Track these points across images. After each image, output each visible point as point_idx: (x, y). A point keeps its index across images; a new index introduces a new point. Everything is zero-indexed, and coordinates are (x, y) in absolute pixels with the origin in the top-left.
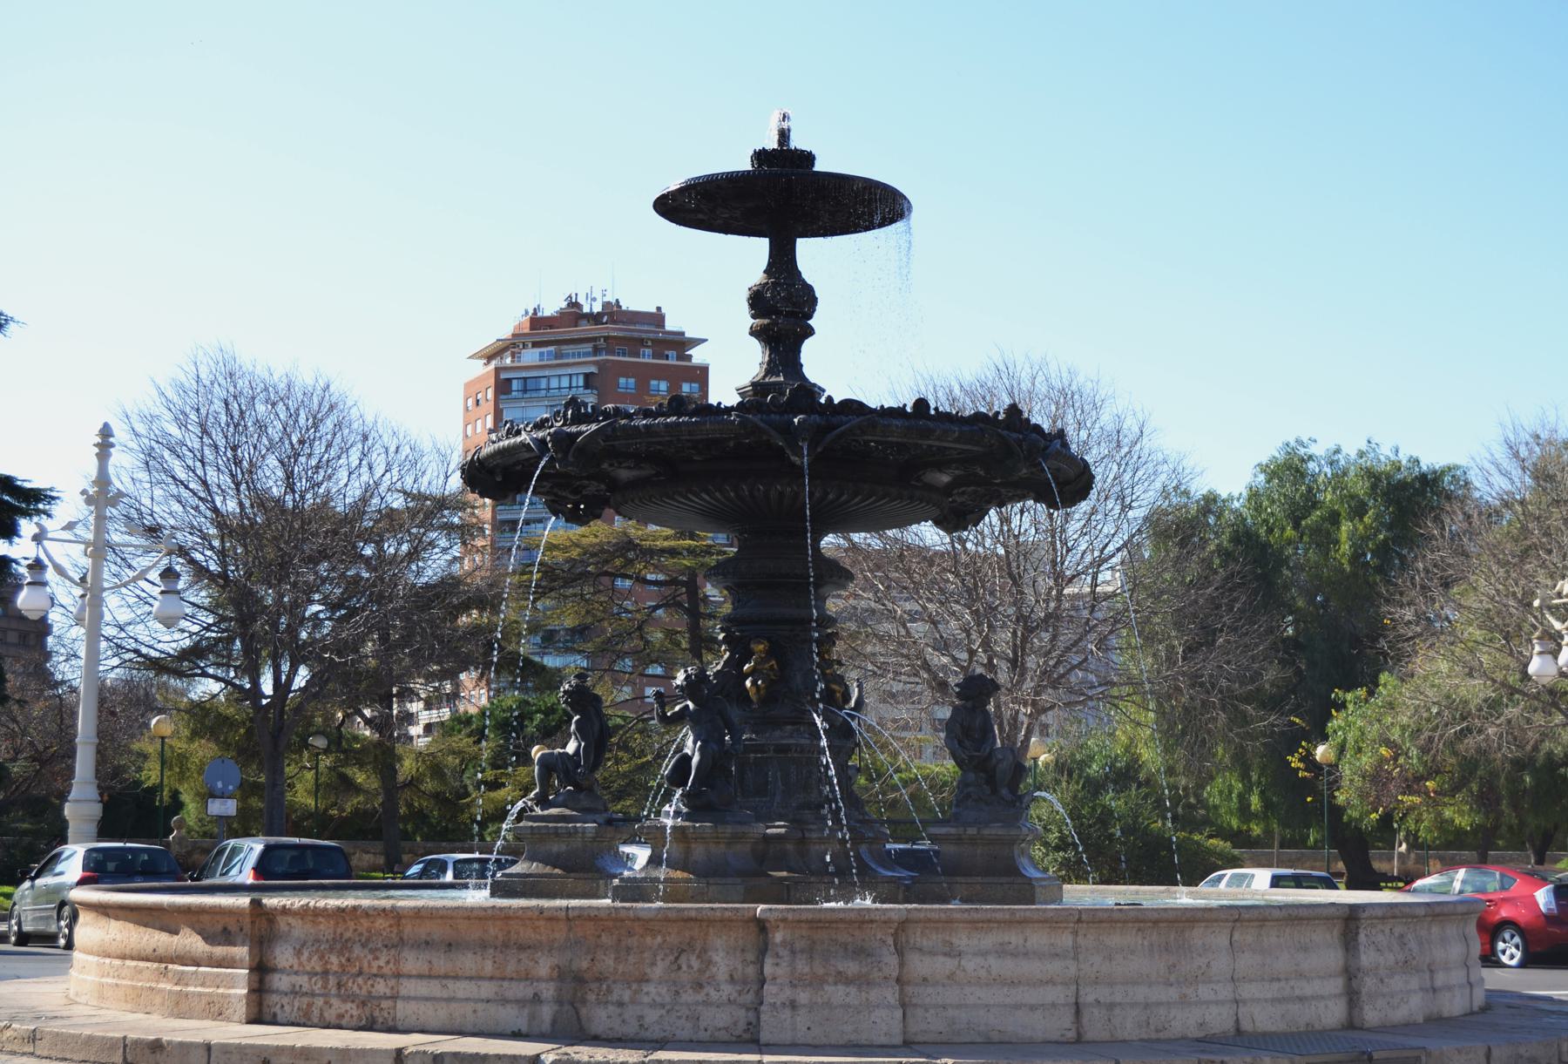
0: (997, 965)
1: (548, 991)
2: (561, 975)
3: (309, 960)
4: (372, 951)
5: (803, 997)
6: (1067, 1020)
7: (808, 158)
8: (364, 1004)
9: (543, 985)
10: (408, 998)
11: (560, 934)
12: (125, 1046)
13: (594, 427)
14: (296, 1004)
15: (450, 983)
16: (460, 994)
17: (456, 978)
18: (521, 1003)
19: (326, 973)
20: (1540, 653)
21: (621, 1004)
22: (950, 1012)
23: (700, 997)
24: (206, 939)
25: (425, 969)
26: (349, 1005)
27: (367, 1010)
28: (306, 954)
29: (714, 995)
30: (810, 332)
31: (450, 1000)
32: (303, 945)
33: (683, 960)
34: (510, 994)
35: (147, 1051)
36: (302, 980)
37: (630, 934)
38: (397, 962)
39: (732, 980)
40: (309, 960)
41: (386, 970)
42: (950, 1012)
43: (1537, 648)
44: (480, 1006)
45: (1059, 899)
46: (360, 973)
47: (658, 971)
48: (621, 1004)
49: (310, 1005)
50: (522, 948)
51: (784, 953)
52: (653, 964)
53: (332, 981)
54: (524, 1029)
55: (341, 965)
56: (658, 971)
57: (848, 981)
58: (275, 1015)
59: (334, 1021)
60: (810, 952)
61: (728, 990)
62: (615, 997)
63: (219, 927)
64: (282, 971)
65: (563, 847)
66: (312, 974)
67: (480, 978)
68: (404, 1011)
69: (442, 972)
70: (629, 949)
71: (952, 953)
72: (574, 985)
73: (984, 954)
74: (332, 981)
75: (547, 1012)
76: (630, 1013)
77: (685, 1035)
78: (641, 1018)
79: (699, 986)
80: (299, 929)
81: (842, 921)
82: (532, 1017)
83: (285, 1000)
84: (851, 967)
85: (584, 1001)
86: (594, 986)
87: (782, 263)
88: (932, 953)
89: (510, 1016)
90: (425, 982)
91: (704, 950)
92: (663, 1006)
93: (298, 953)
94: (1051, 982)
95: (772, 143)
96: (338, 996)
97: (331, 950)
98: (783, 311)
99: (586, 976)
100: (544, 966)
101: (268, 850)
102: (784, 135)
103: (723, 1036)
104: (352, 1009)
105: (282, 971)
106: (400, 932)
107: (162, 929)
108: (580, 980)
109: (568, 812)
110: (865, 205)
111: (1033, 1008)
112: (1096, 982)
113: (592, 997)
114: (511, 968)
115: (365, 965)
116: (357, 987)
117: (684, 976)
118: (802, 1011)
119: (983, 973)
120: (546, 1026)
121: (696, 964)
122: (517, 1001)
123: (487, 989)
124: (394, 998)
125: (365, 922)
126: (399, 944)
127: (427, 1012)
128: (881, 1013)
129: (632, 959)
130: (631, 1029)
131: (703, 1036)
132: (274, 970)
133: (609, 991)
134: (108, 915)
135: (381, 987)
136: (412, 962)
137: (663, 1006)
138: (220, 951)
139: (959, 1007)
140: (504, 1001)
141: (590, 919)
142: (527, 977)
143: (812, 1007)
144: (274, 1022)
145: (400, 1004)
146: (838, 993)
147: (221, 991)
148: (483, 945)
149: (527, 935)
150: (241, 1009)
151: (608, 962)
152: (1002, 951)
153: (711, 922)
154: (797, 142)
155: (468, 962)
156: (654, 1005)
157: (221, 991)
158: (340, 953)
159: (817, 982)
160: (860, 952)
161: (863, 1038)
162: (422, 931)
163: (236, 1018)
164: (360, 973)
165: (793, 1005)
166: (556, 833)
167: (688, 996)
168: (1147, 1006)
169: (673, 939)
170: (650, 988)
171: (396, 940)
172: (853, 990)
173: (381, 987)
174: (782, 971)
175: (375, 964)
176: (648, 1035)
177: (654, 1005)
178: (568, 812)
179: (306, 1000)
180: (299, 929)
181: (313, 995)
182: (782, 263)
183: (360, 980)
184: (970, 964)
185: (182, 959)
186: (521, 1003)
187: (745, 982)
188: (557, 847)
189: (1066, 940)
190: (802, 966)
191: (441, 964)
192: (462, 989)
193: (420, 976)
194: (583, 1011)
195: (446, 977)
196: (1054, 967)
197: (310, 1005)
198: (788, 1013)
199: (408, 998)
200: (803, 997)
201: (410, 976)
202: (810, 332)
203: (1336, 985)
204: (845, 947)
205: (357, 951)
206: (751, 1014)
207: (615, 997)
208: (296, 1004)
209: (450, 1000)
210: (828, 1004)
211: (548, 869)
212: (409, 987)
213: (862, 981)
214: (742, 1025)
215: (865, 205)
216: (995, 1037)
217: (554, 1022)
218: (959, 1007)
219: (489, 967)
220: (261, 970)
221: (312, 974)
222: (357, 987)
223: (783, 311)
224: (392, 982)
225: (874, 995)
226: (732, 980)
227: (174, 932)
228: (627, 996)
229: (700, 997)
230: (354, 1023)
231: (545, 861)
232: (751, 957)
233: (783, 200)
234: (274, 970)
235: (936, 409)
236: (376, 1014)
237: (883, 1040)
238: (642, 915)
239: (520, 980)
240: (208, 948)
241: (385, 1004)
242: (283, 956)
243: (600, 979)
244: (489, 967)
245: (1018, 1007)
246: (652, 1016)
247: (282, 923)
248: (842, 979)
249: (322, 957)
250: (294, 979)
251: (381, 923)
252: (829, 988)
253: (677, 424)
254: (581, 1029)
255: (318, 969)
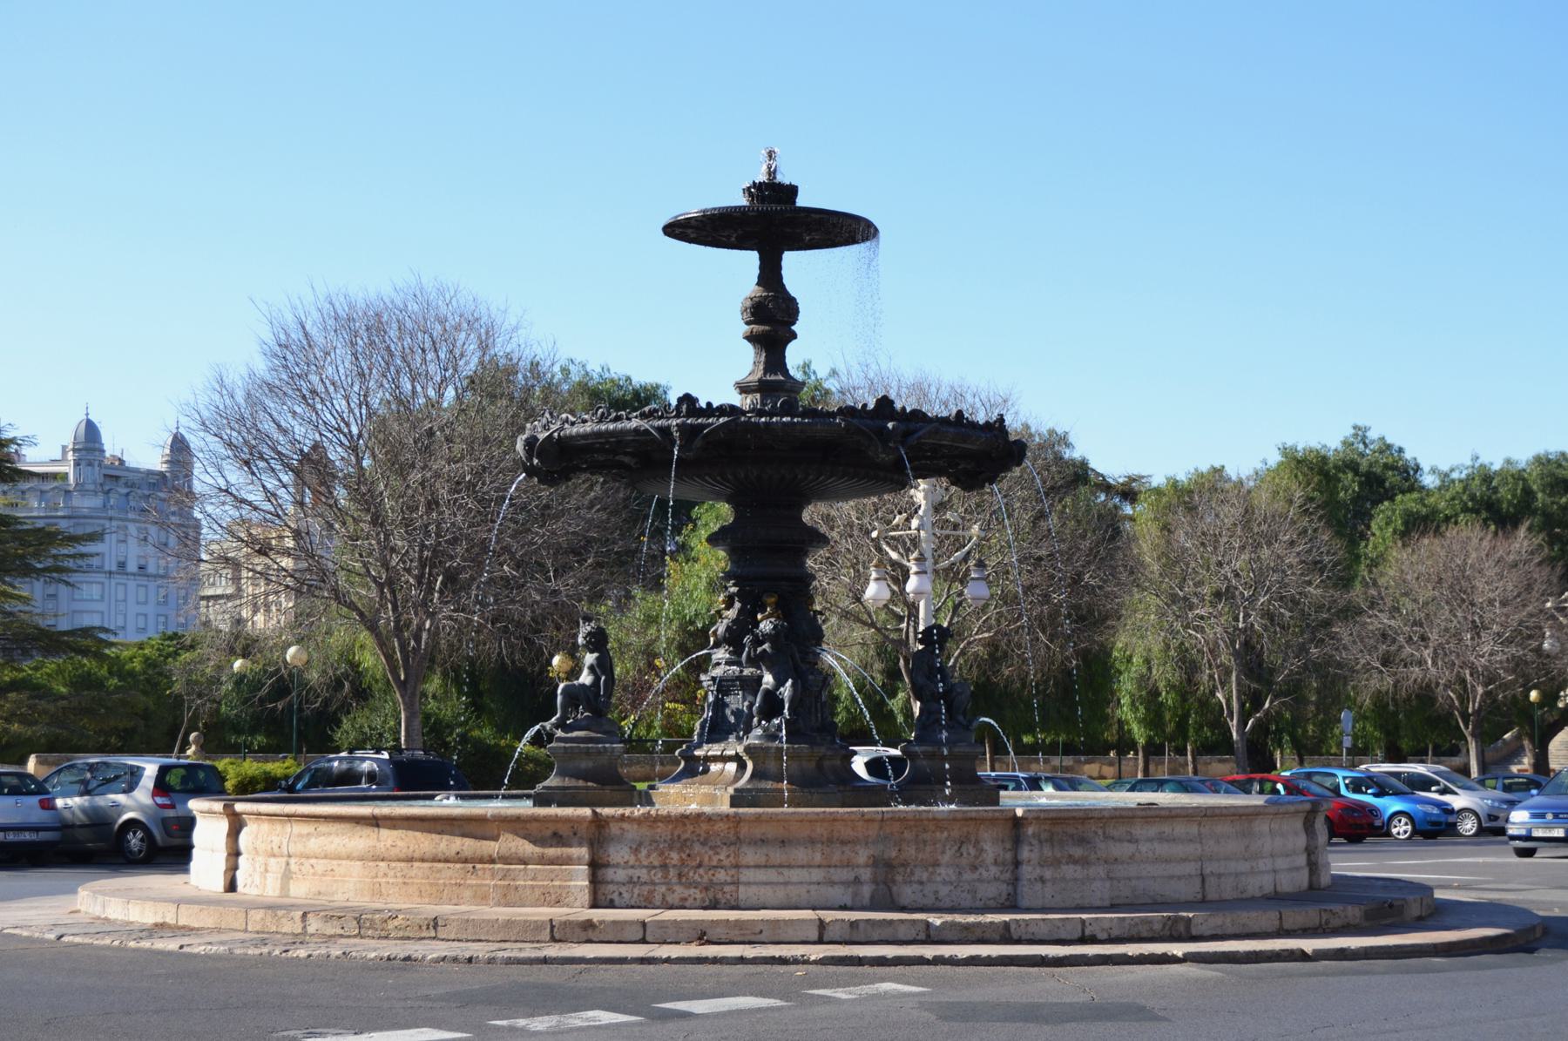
0: (1162, 849)
1: (866, 874)
2: (875, 862)
3: (648, 856)
4: (711, 848)
5: (1048, 874)
6: (1305, 873)
7: (792, 191)
8: (707, 889)
9: (862, 871)
10: (749, 884)
11: (873, 831)
12: (552, 927)
13: (721, 420)
14: (636, 891)
15: (786, 871)
16: (795, 879)
17: (789, 867)
18: (846, 884)
19: (664, 866)
20: (877, 579)
21: (921, 883)
22: (1134, 882)
23: (976, 876)
24: (534, 842)
25: (763, 860)
26: (692, 891)
27: (711, 895)
28: (644, 852)
29: (985, 874)
30: (794, 336)
31: (786, 884)
32: (640, 844)
33: (964, 850)
34: (835, 878)
35: (578, 930)
36: (636, 873)
37: (925, 831)
38: (737, 855)
39: (996, 863)
40: (648, 856)
41: (726, 863)
42: (1134, 882)
43: (874, 575)
44: (813, 888)
45: (996, 802)
46: (700, 866)
47: (946, 858)
48: (921, 883)
49: (651, 892)
50: (843, 843)
51: (1035, 842)
52: (943, 852)
53: (672, 872)
54: (849, 904)
55: (682, 860)
56: (946, 858)
57: (1076, 862)
58: (612, 901)
59: (677, 902)
60: (1051, 840)
61: (994, 870)
62: (916, 878)
63: (549, 833)
64: (617, 866)
65: (590, 764)
66: (651, 867)
67: (810, 866)
68: (744, 893)
69: (778, 862)
70: (925, 842)
71: (1133, 840)
72: (886, 870)
73: (1151, 840)
74: (672, 872)
75: (866, 891)
76: (929, 889)
77: (967, 904)
78: (936, 892)
79: (974, 868)
80: (632, 831)
81: (1074, 818)
82: (855, 894)
83: (623, 889)
84: (1077, 852)
85: (894, 882)
86: (901, 870)
87: (770, 275)
88: (1120, 840)
89: (839, 894)
90: (762, 871)
91: (977, 842)
92: (951, 883)
93: (636, 851)
94: (1184, 860)
95: (762, 177)
96: (680, 883)
97: (671, 848)
98: (773, 319)
99: (895, 863)
100: (863, 856)
101: (164, 771)
102: (772, 173)
103: (992, 903)
104: (697, 894)
105: (617, 866)
106: (736, 833)
107: (464, 835)
108: (889, 865)
109: (593, 735)
110: (840, 230)
111: (1179, 878)
112: (1211, 859)
113: (899, 878)
114: (836, 857)
115: (706, 859)
116: (701, 876)
117: (964, 861)
118: (1049, 884)
119: (1150, 854)
120: (866, 901)
121: (973, 851)
122: (842, 883)
123: (817, 875)
124: (736, 883)
125: (704, 826)
126: (738, 841)
127: (766, 894)
128: (1098, 884)
129: (928, 849)
130: (929, 901)
131: (979, 904)
132: (607, 865)
133: (912, 873)
134: (378, 826)
135: (721, 876)
136: (750, 856)
137: (951, 883)
138: (552, 852)
139: (1138, 878)
140: (832, 883)
141: (899, 820)
142: (848, 865)
143: (1054, 881)
144: (611, 905)
145: (742, 888)
146: (1070, 871)
147: (557, 883)
148: (812, 841)
149: (847, 833)
150: (585, 897)
151: (910, 852)
152: (1161, 838)
153: (983, 820)
154: (784, 178)
155: (800, 854)
156: (945, 883)
157: (557, 883)
158: (681, 850)
159: (1056, 863)
160: (1082, 841)
161: (1086, 903)
162: (758, 832)
163: (578, 903)
164: (700, 866)
165: (1042, 880)
166: (587, 752)
167: (968, 876)
168: (1237, 875)
169: (956, 834)
170: (942, 870)
171: (733, 838)
172: (1078, 868)
173: (721, 876)
174: (1035, 856)
175: (715, 859)
176: (941, 905)
177: (945, 883)
178: (593, 735)
179: (646, 888)
180: (632, 831)
181: (653, 883)
182: (770, 275)
183: (701, 871)
184: (1144, 848)
185: (506, 860)
186: (846, 884)
187: (1004, 864)
188: (585, 764)
189: (1194, 829)
190: (1047, 852)
191: (777, 856)
192: (795, 875)
193: (757, 867)
194: (895, 889)
195: (781, 866)
196: (1191, 849)
197: (651, 892)
198: (1039, 886)
199: (749, 884)
200: (1048, 874)
201: (748, 867)
202: (794, 336)
203: (1302, 860)
204: (1072, 836)
205: (697, 848)
206: (1010, 888)
207: (916, 878)
208: (636, 891)
209: (786, 884)
210: (1063, 879)
211: (581, 783)
212: (748, 875)
213: (1084, 862)
214: (1004, 896)
215: (840, 230)
216: (1159, 900)
217: (872, 897)
218: (1138, 878)
219: (818, 858)
220: (596, 866)
221: (651, 867)
222: (701, 876)
223: (773, 319)
224: (733, 872)
225: (1092, 871)
226: (996, 863)
227: (495, 838)
228: (925, 876)
229: (976, 876)
230: (698, 903)
231: (577, 775)
232: (1008, 846)
233: (772, 223)
234: (607, 865)
235: (744, 389)
236: (720, 896)
237: (1098, 903)
238: (940, 816)
239: (842, 867)
240: (538, 850)
241: (727, 889)
242: (618, 854)
243: (904, 865)
244: (818, 858)
245: (1171, 877)
246: (944, 891)
247: (614, 829)
248: (1073, 861)
249: (662, 854)
250: (631, 872)
251: (720, 826)
252: (1064, 867)
253: (792, 424)
254: (893, 901)
255: (656, 863)
